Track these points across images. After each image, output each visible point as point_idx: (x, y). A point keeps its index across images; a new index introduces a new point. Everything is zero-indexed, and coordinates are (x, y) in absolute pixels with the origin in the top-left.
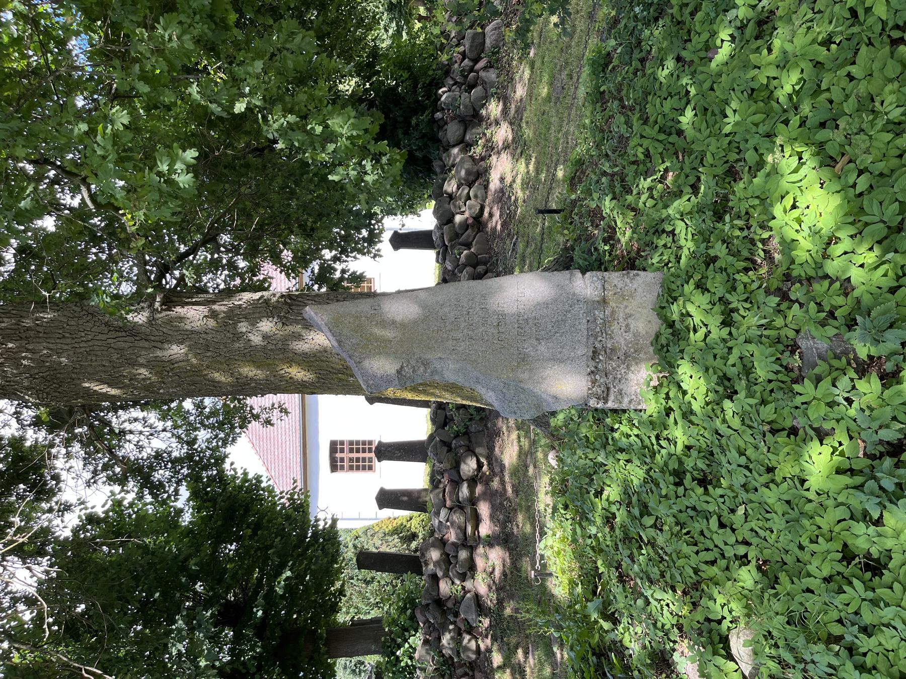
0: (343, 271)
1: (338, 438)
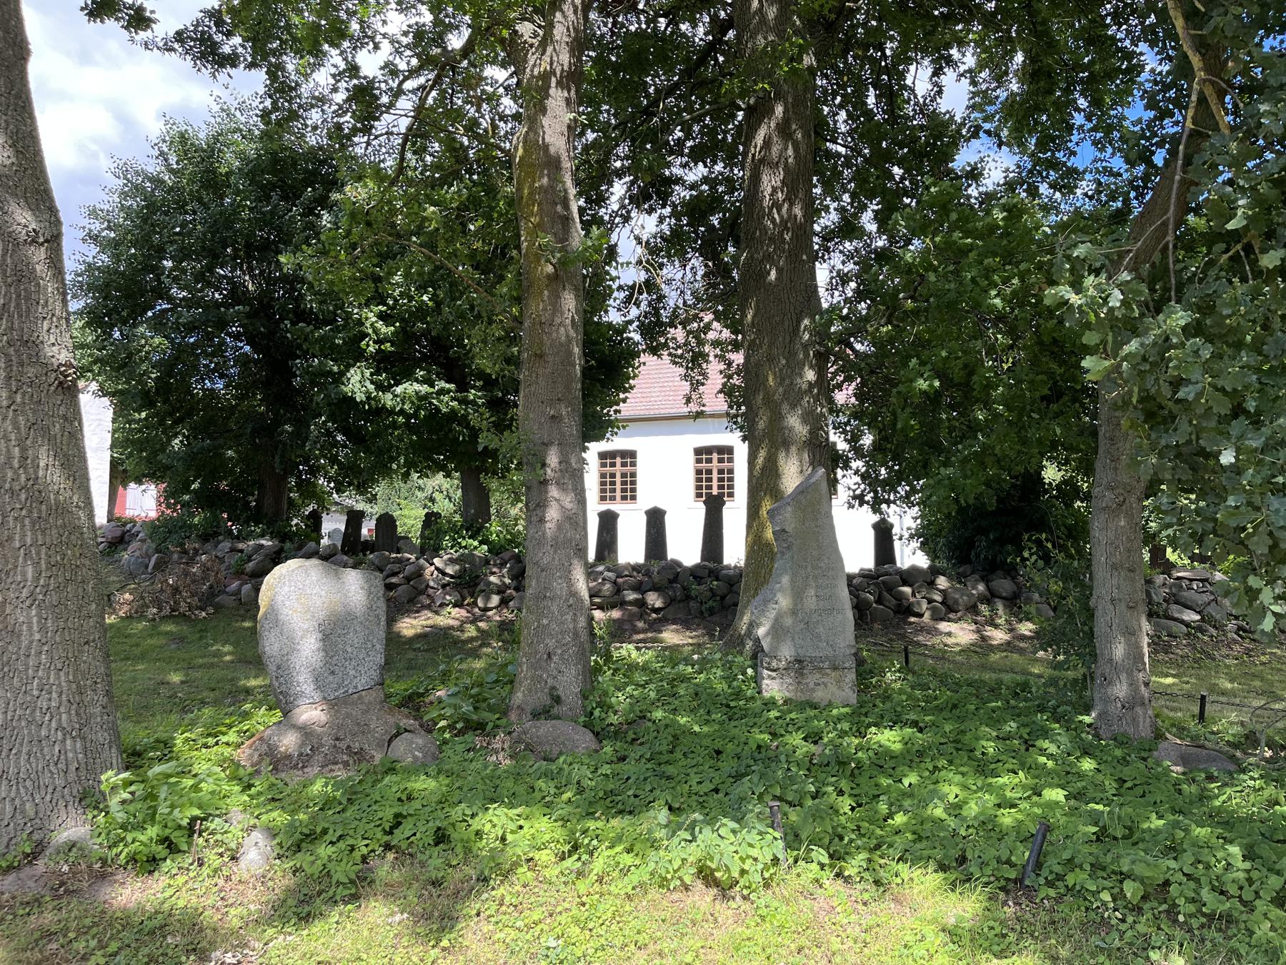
0: (1141, 54)
1: (639, 460)
